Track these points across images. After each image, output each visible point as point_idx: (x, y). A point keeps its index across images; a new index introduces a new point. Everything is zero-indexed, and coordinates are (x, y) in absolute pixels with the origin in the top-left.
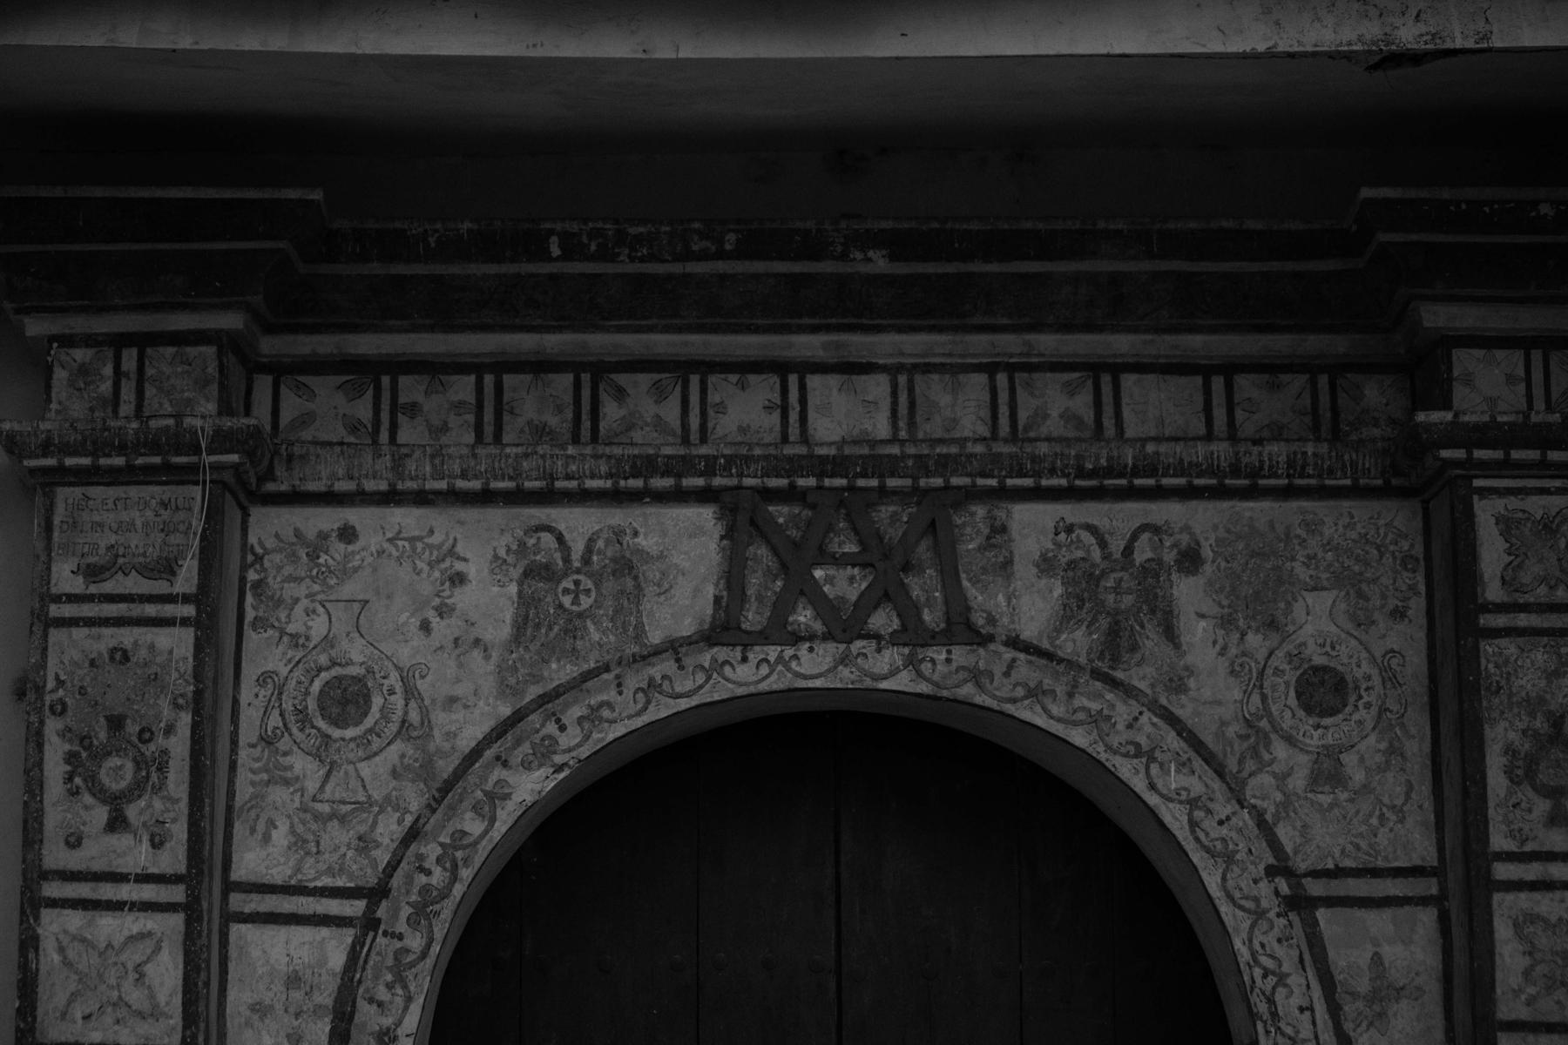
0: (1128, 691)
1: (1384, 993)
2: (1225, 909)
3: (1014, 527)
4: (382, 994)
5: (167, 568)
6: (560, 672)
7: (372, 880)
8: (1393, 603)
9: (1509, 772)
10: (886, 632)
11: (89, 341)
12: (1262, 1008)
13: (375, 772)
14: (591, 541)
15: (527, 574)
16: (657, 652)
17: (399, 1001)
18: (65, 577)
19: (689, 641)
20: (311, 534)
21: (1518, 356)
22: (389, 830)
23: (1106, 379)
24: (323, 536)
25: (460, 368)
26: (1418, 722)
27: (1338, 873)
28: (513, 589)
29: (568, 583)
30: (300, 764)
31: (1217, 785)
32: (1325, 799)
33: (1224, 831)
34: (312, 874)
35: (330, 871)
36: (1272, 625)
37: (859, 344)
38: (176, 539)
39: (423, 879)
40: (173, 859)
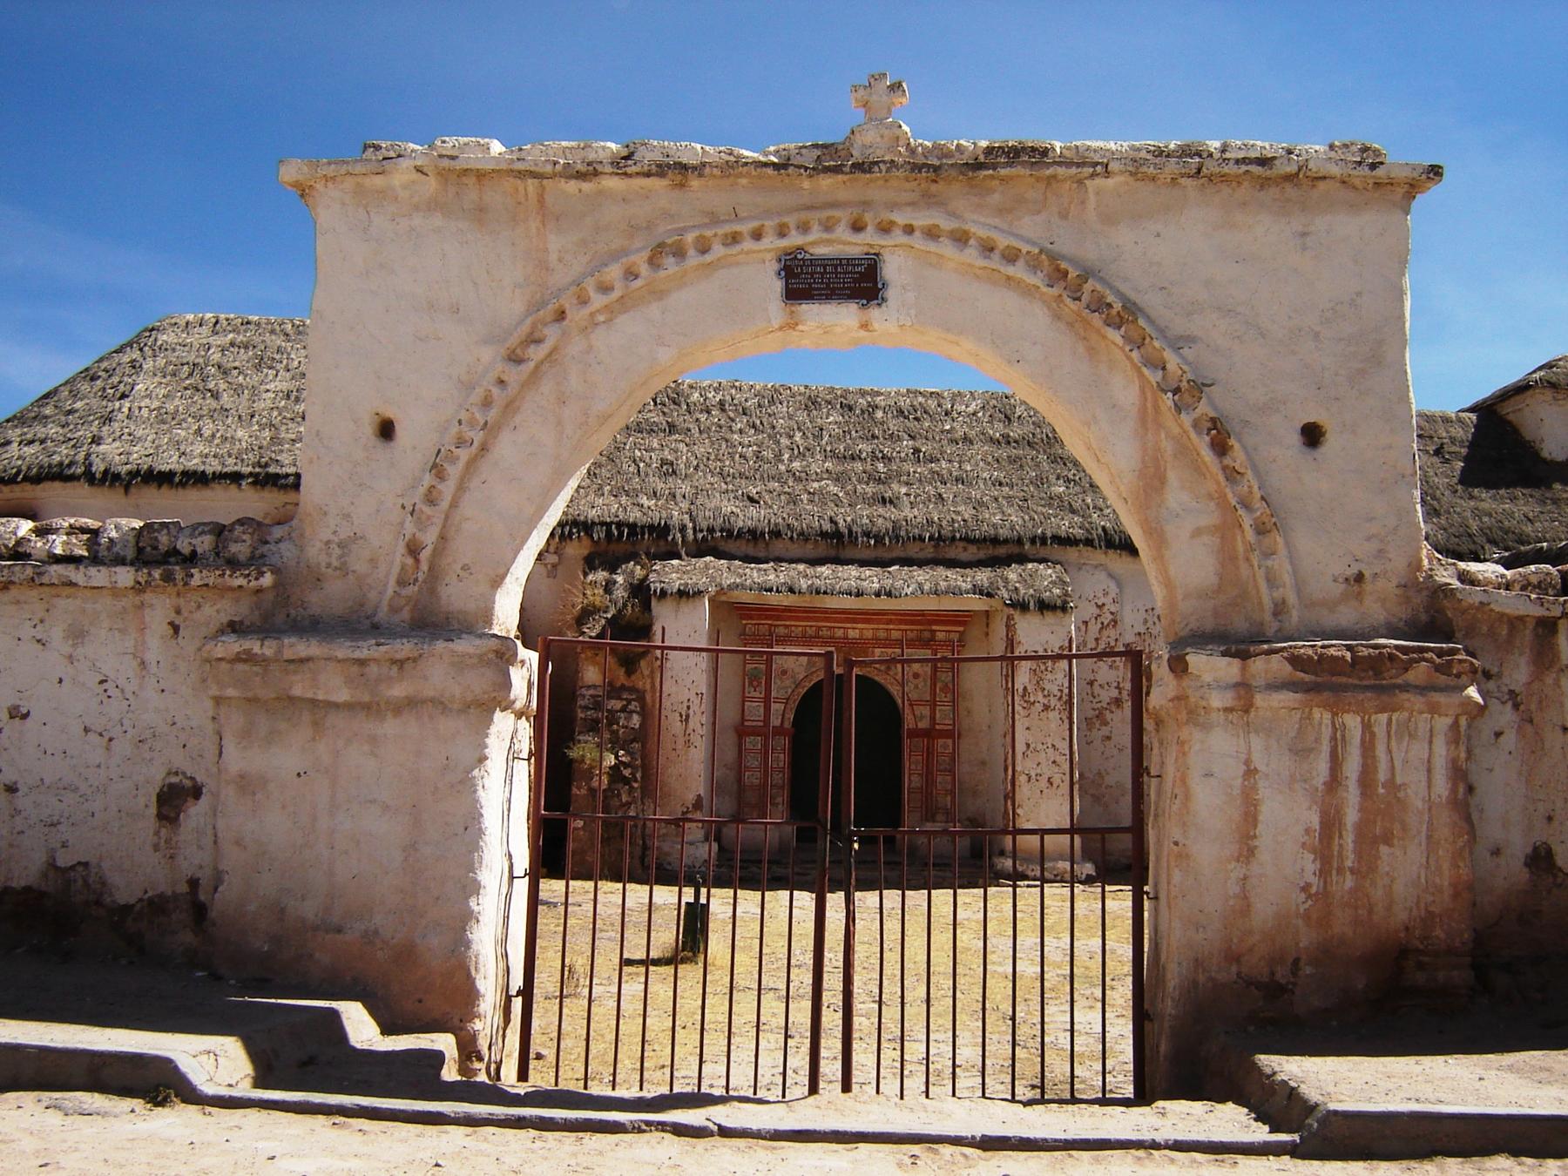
6: (814, 669)
22: (790, 691)
37: (855, 625)
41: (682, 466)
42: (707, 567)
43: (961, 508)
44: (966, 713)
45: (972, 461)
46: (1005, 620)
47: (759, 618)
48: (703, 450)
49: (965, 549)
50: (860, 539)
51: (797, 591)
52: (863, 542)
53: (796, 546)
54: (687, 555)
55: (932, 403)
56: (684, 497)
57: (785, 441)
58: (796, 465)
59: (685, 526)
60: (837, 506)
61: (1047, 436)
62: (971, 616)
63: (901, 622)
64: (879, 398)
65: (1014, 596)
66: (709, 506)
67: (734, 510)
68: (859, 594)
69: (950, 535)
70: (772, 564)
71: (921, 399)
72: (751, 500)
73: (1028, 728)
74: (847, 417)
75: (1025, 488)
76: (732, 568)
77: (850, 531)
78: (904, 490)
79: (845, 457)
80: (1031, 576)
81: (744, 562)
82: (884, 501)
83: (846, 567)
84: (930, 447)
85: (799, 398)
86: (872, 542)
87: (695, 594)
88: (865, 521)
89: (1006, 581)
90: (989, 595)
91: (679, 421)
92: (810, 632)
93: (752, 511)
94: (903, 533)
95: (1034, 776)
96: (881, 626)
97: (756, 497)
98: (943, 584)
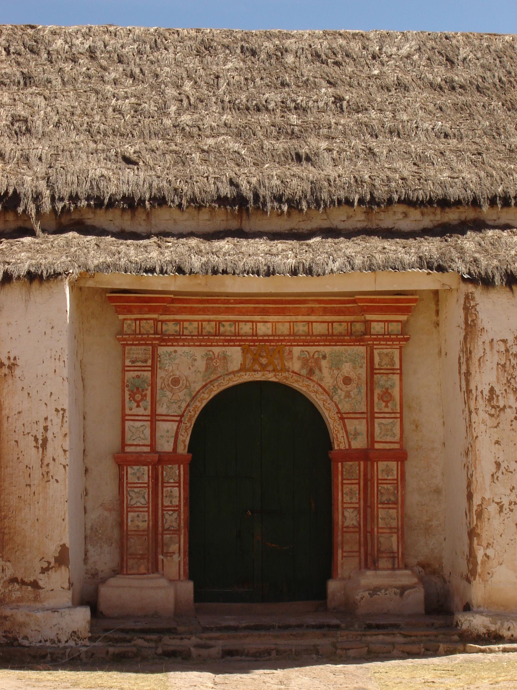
0: (313, 381)
2: (329, 419)
3: (293, 351)
4: (183, 434)
5: (146, 361)
6: (213, 377)
7: (181, 413)
8: (360, 365)
9: (378, 398)
10: (271, 370)
11: (131, 319)
12: (335, 436)
14: (219, 353)
15: (207, 359)
16: (230, 373)
17: (186, 435)
18: (128, 363)
19: (236, 372)
20: (169, 352)
21: (383, 323)
22: (184, 405)
23: (310, 324)
24: (171, 352)
25: (195, 321)
26: (364, 387)
27: (349, 413)
28: (205, 362)
29: (215, 361)
30: (168, 393)
31: (328, 397)
32: (347, 400)
33: (329, 406)
34: (170, 413)
35: (174, 412)
36: (338, 369)
37: (266, 318)
38: (148, 356)
39: (190, 413)
40: (148, 412)
41: (39, 123)
42: (68, 244)
43: (398, 165)
44: (413, 427)
45: (409, 109)
46: (462, 301)
47: (141, 310)
48: (65, 103)
49: (406, 215)
50: (269, 205)
51: (187, 271)
52: (273, 208)
53: (186, 216)
54: (43, 231)
55: (355, 46)
56: (40, 159)
57: (171, 92)
58: (186, 118)
59: (41, 194)
60: (238, 165)
61: (500, 80)
62: (416, 300)
63: (326, 311)
64: (289, 41)
65: (474, 269)
66: (71, 167)
67: (105, 172)
68: (270, 273)
69: (386, 197)
70: (154, 239)
71: (341, 41)
72: (127, 160)
73: (497, 442)
74: (249, 63)
75: (478, 140)
76: (102, 245)
77: (256, 196)
78: (324, 145)
79: (248, 109)
80: (492, 244)
81: (118, 238)
82: (299, 158)
83: (252, 241)
84: (355, 95)
85: (189, 43)
86: (285, 208)
87: (49, 277)
88: (275, 182)
89: (461, 251)
90: (441, 269)
91: (37, 72)
92: (209, 328)
93: (129, 173)
94: (325, 196)
95: (506, 506)
96: (300, 318)
97: (134, 157)
98: (379, 258)
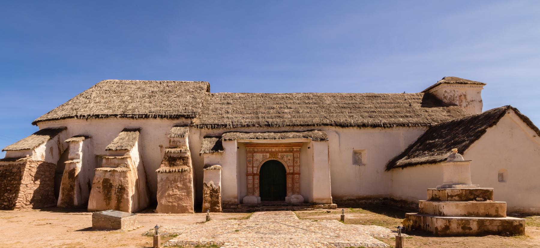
1: (291, 170)
13: (258, 163)
22: (258, 164)
